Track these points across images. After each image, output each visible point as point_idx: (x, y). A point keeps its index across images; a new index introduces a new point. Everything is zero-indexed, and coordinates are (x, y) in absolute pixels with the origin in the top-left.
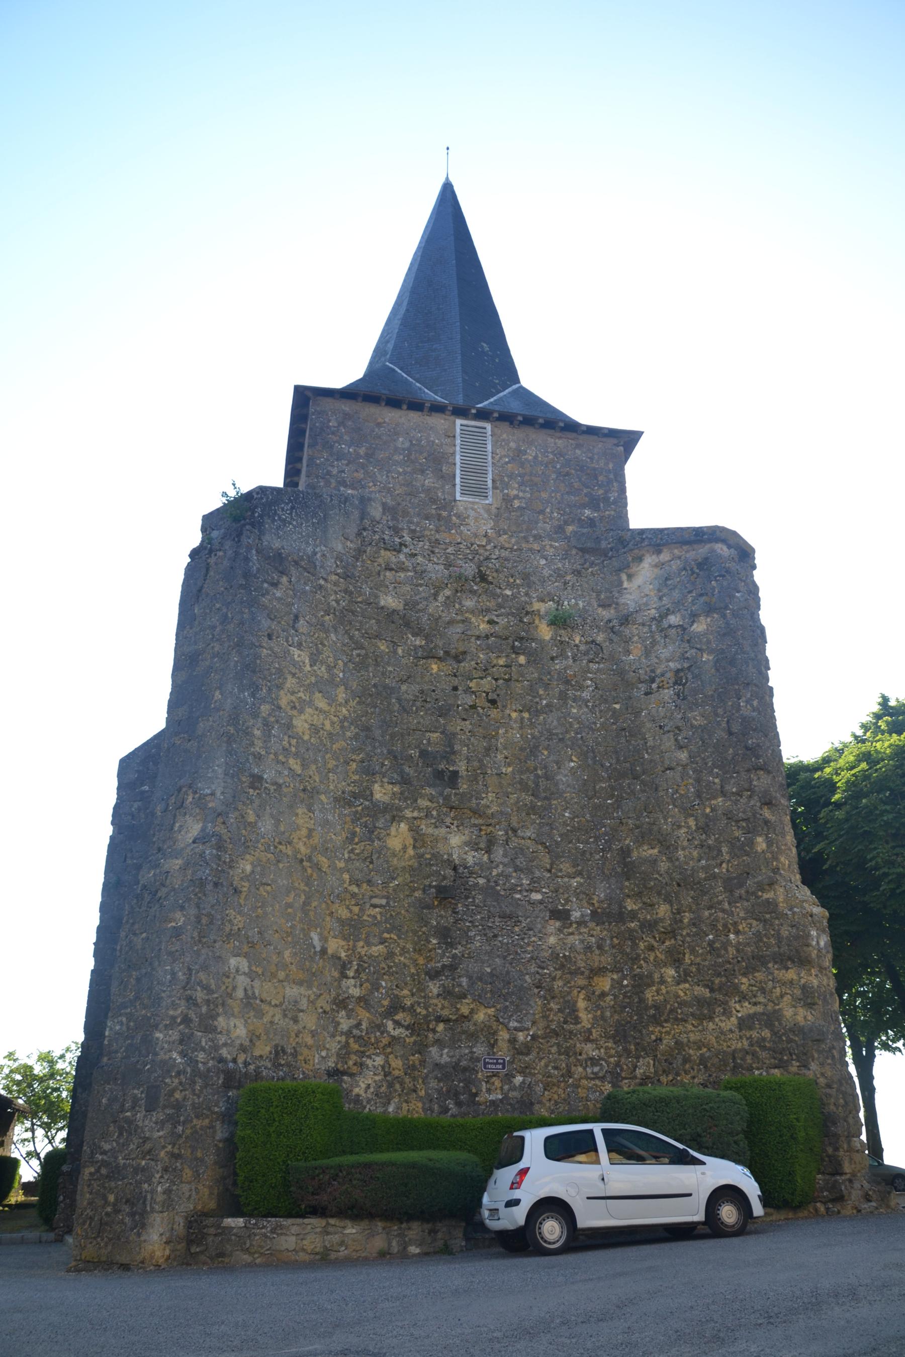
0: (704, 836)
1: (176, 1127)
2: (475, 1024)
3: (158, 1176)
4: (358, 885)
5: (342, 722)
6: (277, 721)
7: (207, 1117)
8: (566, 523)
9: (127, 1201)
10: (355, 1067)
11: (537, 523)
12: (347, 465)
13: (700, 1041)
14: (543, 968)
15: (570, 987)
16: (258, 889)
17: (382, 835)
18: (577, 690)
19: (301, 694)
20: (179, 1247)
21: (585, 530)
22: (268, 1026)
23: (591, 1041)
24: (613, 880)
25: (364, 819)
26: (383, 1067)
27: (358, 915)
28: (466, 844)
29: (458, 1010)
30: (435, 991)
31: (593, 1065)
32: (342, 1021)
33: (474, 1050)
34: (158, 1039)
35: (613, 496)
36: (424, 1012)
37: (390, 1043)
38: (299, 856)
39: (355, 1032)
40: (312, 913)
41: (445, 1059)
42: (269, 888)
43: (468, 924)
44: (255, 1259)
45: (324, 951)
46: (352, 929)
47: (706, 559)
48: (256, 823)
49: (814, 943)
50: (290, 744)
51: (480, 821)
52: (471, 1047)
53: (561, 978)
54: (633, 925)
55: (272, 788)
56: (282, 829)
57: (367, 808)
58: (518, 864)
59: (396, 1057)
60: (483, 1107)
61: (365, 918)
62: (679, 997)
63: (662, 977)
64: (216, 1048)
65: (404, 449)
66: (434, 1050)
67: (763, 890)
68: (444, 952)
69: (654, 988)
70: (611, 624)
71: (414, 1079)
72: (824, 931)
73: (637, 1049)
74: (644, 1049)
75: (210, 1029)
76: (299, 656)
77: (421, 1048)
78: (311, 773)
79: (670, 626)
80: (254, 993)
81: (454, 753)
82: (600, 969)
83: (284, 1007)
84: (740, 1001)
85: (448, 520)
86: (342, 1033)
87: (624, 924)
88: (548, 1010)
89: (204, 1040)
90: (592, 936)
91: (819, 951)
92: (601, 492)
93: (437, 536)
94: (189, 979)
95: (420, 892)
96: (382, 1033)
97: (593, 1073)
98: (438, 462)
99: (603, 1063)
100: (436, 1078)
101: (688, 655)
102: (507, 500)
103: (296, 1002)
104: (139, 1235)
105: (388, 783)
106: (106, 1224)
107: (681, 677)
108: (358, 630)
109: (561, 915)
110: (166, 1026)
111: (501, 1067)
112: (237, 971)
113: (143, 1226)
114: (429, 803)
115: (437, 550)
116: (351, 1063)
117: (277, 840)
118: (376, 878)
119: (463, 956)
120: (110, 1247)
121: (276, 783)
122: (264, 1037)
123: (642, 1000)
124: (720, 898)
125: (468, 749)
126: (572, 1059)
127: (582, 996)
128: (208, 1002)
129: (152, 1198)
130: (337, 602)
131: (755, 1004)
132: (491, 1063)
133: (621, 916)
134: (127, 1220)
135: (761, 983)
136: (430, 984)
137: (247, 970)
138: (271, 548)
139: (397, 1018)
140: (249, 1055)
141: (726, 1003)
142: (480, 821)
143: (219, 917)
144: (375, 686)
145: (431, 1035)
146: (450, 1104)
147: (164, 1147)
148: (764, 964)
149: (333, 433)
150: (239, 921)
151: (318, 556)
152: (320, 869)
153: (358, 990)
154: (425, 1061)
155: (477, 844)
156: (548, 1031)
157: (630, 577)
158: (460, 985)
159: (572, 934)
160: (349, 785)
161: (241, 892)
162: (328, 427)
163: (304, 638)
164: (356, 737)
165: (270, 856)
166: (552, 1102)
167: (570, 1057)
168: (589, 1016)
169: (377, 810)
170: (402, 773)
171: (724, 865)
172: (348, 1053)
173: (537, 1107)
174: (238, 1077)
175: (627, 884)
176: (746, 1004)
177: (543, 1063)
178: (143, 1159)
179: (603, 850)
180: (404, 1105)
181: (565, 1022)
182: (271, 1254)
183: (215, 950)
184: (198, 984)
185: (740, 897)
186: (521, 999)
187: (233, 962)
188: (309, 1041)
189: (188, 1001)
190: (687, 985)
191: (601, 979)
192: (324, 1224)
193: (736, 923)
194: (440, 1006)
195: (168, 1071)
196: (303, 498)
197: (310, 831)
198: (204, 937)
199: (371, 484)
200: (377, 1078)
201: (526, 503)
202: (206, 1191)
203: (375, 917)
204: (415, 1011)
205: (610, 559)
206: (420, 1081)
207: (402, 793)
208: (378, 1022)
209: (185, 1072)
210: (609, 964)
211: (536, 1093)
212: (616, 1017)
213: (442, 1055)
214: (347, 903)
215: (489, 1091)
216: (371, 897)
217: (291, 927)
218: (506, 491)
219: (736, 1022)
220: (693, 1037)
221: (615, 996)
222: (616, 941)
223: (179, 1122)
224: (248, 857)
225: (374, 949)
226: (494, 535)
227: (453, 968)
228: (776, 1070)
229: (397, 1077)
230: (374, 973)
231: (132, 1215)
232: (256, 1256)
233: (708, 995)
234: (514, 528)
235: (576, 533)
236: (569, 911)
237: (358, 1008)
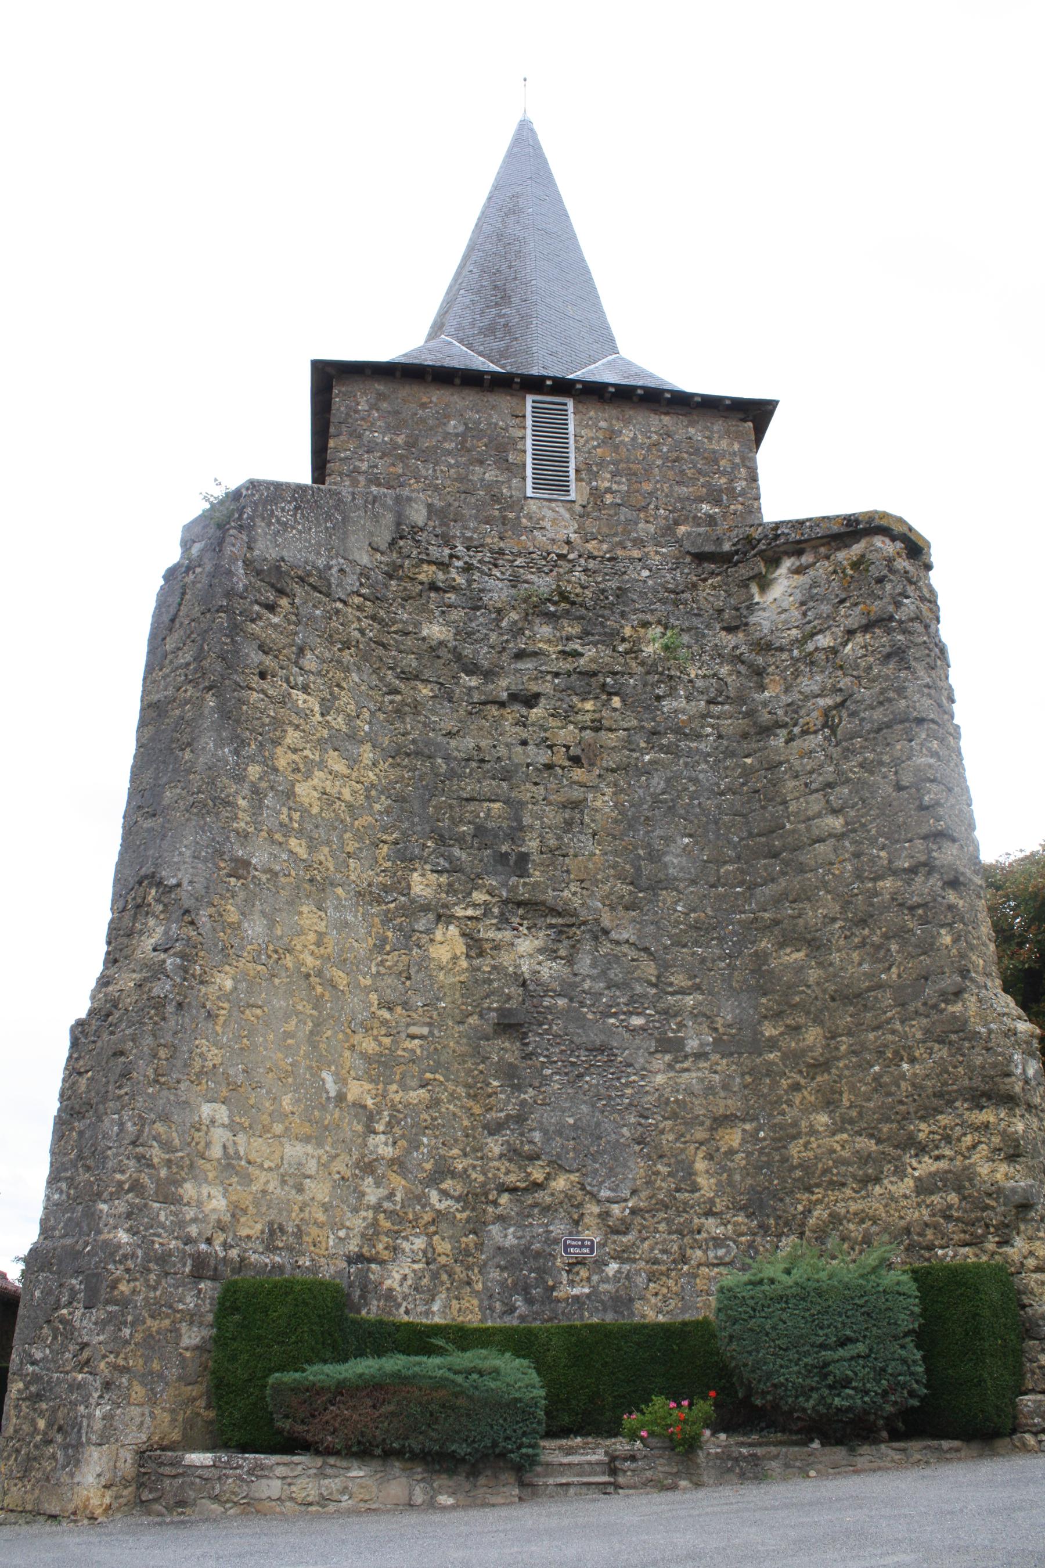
0: (866, 932)
1: (120, 1330)
2: (552, 1194)
3: (96, 1395)
4: (390, 1009)
5: (367, 790)
6: (272, 788)
7: (168, 1316)
8: (677, 523)
9: (60, 1429)
10: (386, 1252)
11: (636, 524)
12: (381, 458)
13: (863, 1211)
14: (647, 1118)
15: (685, 1142)
16: (243, 1013)
17: (423, 941)
18: (692, 741)
19: (307, 752)
20: (125, 1493)
21: (702, 530)
22: (259, 1195)
25: (399, 920)
26: (425, 1252)
27: (390, 1049)
28: (540, 951)
29: (529, 1174)
30: (497, 1150)
31: (717, 1246)
32: (368, 1190)
33: (551, 1228)
34: (101, 1211)
35: (740, 485)
36: (481, 1178)
37: (434, 1220)
39: (386, 1205)
40: (322, 1046)
41: (510, 1241)
42: (259, 1012)
43: (542, 1059)
44: (226, 1510)
45: (341, 1097)
46: (381, 1067)
47: (863, 556)
48: (239, 923)
49: (1019, 1071)
50: (291, 819)
51: (560, 921)
52: (547, 1225)
53: (672, 1130)
54: (772, 1056)
55: (264, 878)
56: (279, 933)
57: (403, 907)
58: (612, 976)
59: (443, 1239)
60: (564, 1305)
61: (400, 1052)
62: (835, 1151)
63: (811, 1126)
64: (182, 1224)
65: (457, 435)
66: (495, 1229)
67: (947, 1002)
68: (508, 1096)
69: (801, 1141)
70: (738, 652)
71: (469, 1268)
72: (1032, 1055)
73: (777, 1224)
74: (787, 1224)
75: (171, 1199)
76: (305, 702)
77: (477, 1226)
78: (322, 858)
79: (817, 649)
80: (237, 1152)
81: (521, 828)
82: (726, 1117)
83: (282, 1170)
84: (916, 1155)
85: (516, 523)
86: (369, 1207)
87: (760, 1055)
88: (654, 1173)
89: (162, 1213)
90: (716, 1072)
91: (1027, 1082)
92: (723, 480)
93: (502, 545)
94: (141, 1132)
95: (476, 1017)
96: (423, 1207)
97: (716, 1257)
98: (502, 451)
99: (731, 1244)
100: (498, 1266)
101: (841, 685)
102: (596, 495)
103: (300, 1164)
104: (72, 1475)
105: (432, 871)
106: (35, 1459)
107: (833, 717)
108: (390, 668)
109: (670, 1046)
110: (111, 1194)
112: (213, 1122)
113: (78, 1462)
114: (488, 897)
115: (500, 562)
116: (380, 1246)
117: (271, 947)
118: (414, 998)
119: (535, 1102)
120: (37, 1491)
121: (270, 871)
122: (252, 1210)
123: (785, 1160)
124: (889, 1014)
125: (543, 823)
126: (687, 1240)
127: (701, 1154)
128: (169, 1163)
129: (88, 1425)
130: (362, 631)
131: (938, 1158)
132: (574, 1246)
133: (758, 1045)
134: (60, 1454)
135: (945, 1128)
136: (489, 1140)
137: (226, 1121)
138: (265, 559)
139: (443, 1186)
140: (231, 1235)
141: (899, 1158)
142: (560, 921)
143: (185, 1048)
144: (414, 741)
145: (490, 1209)
146: (519, 1301)
147: (104, 1357)
148: (950, 1103)
149: (363, 419)
150: (214, 1056)
151: (334, 570)
152: (334, 987)
153: (390, 1149)
154: (482, 1244)
155: (555, 951)
156: (654, 1201)
157: (764, 587)
158: (531, 1142)
159: (687, 1070)
160: (378, 875)
161: (217, 1016)
162: (356, 411)
163: (312, 678)
164: (388, 812)
165: (259, 967)
166: (660, 1297)
167: (684, 1236)
168: (712, 1181)
169: (418, 908)
170: (449, 859)
171: (894, 969)
172: (377, 1233)
173: (638, 1304)
174: (212, 1262)
175: (764, 1000)
176: (926, 1159)
177: (646, 1245)
178: (80, 1372)
179: (730, 956)
180: (454, 1302)
181: (678, 1190)
182: (248, 1504)
183: (179, 1092)
184: (155, 1138)
185: (916, 1012)
186: (616, 1160)
187: (206, 1110)
188: (321, 1217)
189: (139, 1161)
190: (845, 1136)
191: (729, 1131)
192: (320, 1464)
193: (910, 1047)
194: (503, 1170)
195: (112, 1254)
196: (313, 495)
197: (321, 935)
198: (163, 1075)
199: (412, 481)
200: (416, 1266)
201: (622, 498)
202: (167, 1417)
203: (413, 1051)
204: (468, 1176)
205: (736, 565)
206: (476, 1271)
207: (450, 885)
208: (418, 1191)
209: (134, 1255)
210: (738, 1110)
211: (636, 1286)
212: (749, 1181)
213: (506, 1236)
214: (375, 1032)
215: (572, 1283)
216: (408, 1025)
217: (291, 1065)
218: (594, 483)
219: (911, 1183)
220: (854, 1207)
221: (749, 1154)
222: (748, 1079)
223: (125, 1323)
224: (227, 968)
225: (412, 1094)
226: (579, 541)
227: (520, 1119)
228: (967, 1249)
229: (444, 1266)
230: (412, 1126)
231: (65, 1447)
232: (228, 1505)
233: (874, 1148)
234: (605, 530)
235: (689, 534)
237: (390, 1173)
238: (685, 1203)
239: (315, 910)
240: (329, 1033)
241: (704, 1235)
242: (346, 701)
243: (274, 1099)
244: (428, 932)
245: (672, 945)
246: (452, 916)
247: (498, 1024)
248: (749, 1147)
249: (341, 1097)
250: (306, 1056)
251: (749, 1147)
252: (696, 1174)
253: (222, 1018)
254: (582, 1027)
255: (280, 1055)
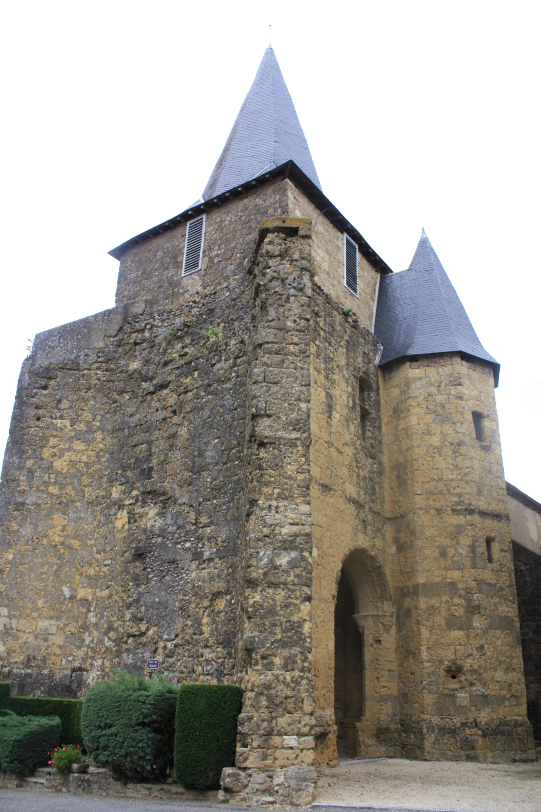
6: (39, 468)
23: (209, 647)
24: (232, 524)
38: (53, 543)
39: (92, 645)
41: (130, 661)
42: (26, 566)
48: (18, 531)
52: (143, 653)
55: (33, 508)
56: (40, 530)
66: (125, 655)
77: (118, 654)
78: (68, 491)
80: (11, 627)
90: (216, 568)
97: (207, 670)
99: (214, 663)
103: (47, 629)
109: (197, 556)
111: (155, 666)
116: (88, 664)
121: (36, 504)
127: (206, 614)
140: (6, 662)
159: (204, 568)
161: (4, 571)
181: (195, 634)
188: (58, 651)
212: (225, 628)
216: (104, 560)
222: (230, 570)
224: (10, 550)
225: (104, 592)
227: (137, 601)
236: (203, 551)
238: (197, 641)
239: (61, 515)
240: (67, 569)
241: (204, 658)
242: (87, 415)
243: (33, 603)
244: (115, 514)
245: (203, 501)
246: (124, 505)
247: (135, 555)
248: (227, 609)
249: (73, 598)
250: (53, 581)
251: (227, 609)
252: (202, 625)
253: (6, 572)
254: (166, 551)
255: (38, 583)
